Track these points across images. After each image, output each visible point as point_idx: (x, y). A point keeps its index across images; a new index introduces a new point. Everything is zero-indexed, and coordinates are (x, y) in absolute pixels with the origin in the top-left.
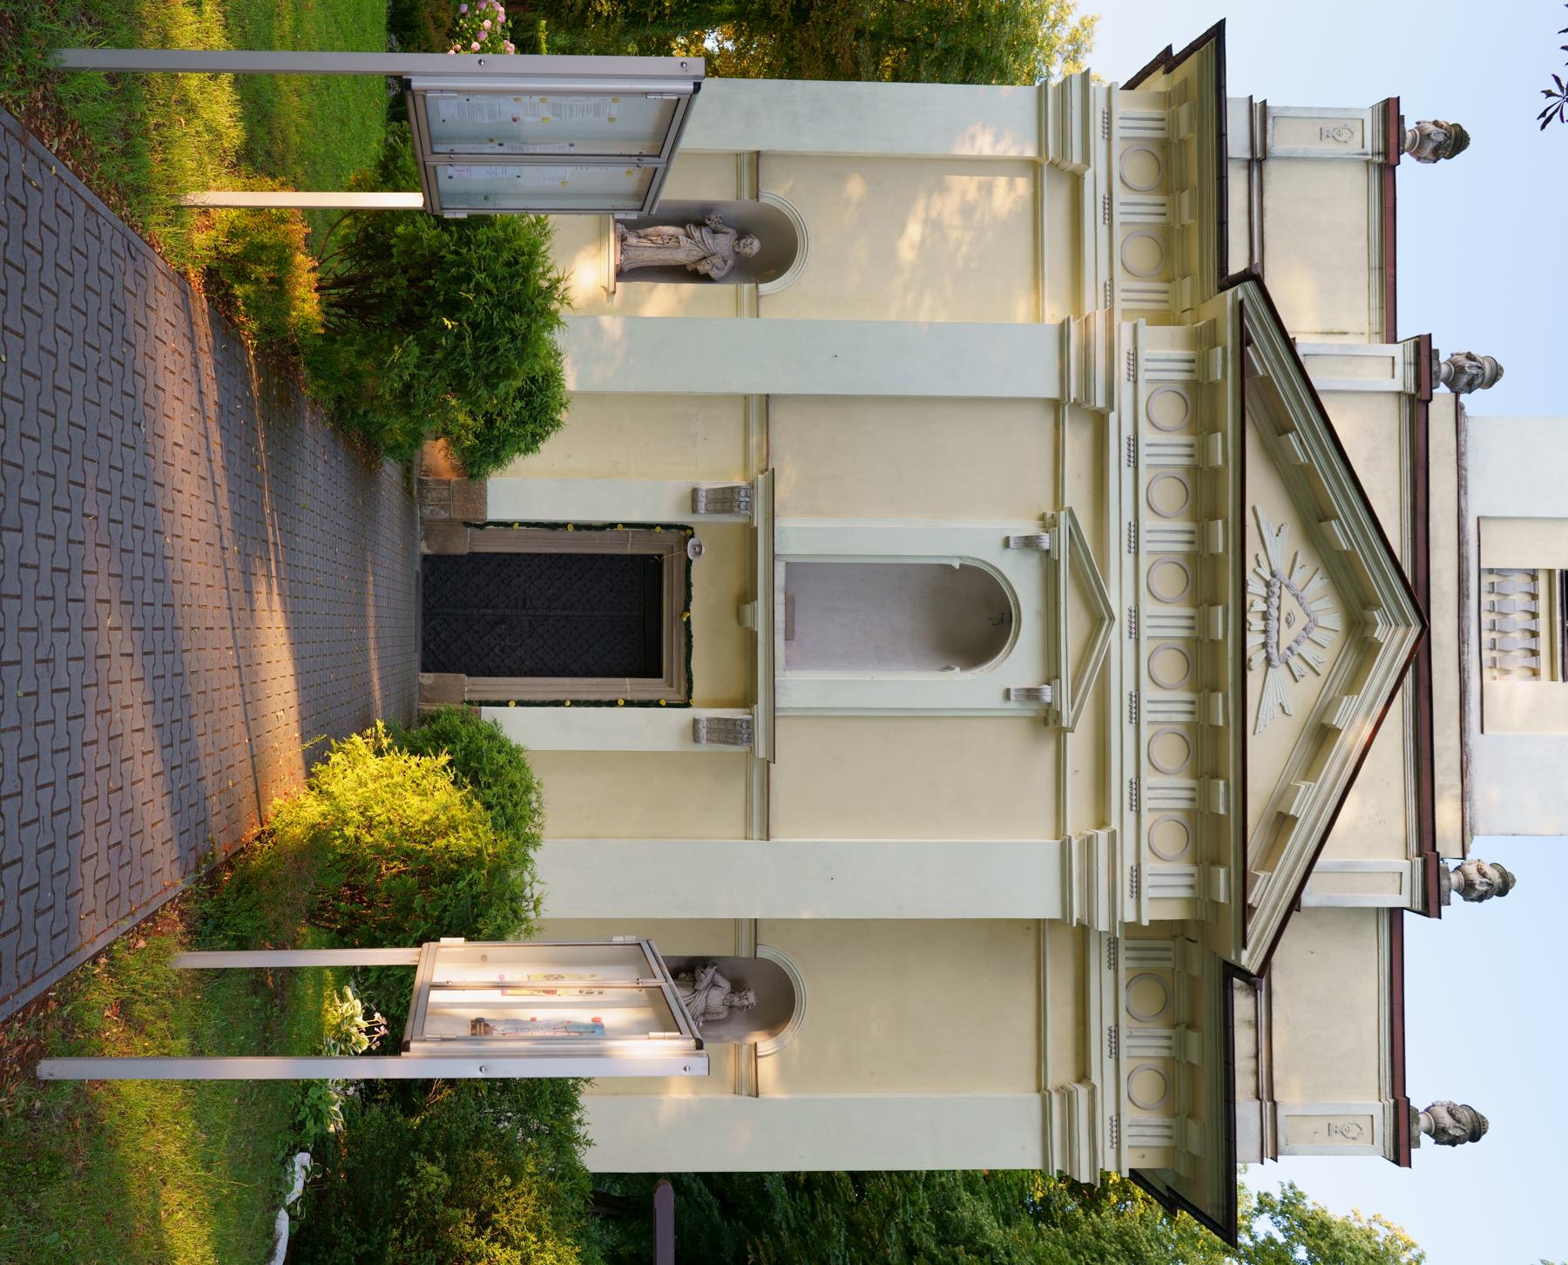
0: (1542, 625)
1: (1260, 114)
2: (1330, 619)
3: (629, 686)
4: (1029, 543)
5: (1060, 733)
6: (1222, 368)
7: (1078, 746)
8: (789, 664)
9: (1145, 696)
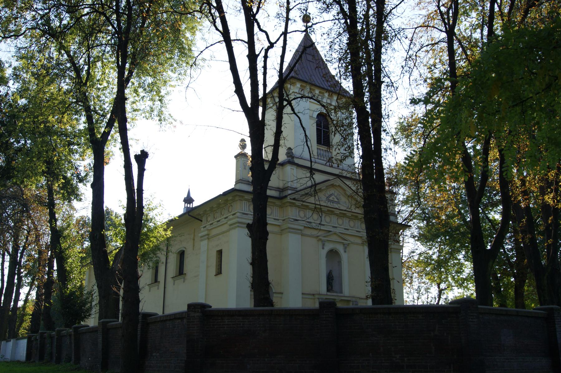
0: (321, 148)
1: (237, 182)
2: (332, 191)
4: (323, 245)
5: (352, 243)
6: (298, 203)
7: (352, 239)
8: (341, 292)
9: (275, 218)
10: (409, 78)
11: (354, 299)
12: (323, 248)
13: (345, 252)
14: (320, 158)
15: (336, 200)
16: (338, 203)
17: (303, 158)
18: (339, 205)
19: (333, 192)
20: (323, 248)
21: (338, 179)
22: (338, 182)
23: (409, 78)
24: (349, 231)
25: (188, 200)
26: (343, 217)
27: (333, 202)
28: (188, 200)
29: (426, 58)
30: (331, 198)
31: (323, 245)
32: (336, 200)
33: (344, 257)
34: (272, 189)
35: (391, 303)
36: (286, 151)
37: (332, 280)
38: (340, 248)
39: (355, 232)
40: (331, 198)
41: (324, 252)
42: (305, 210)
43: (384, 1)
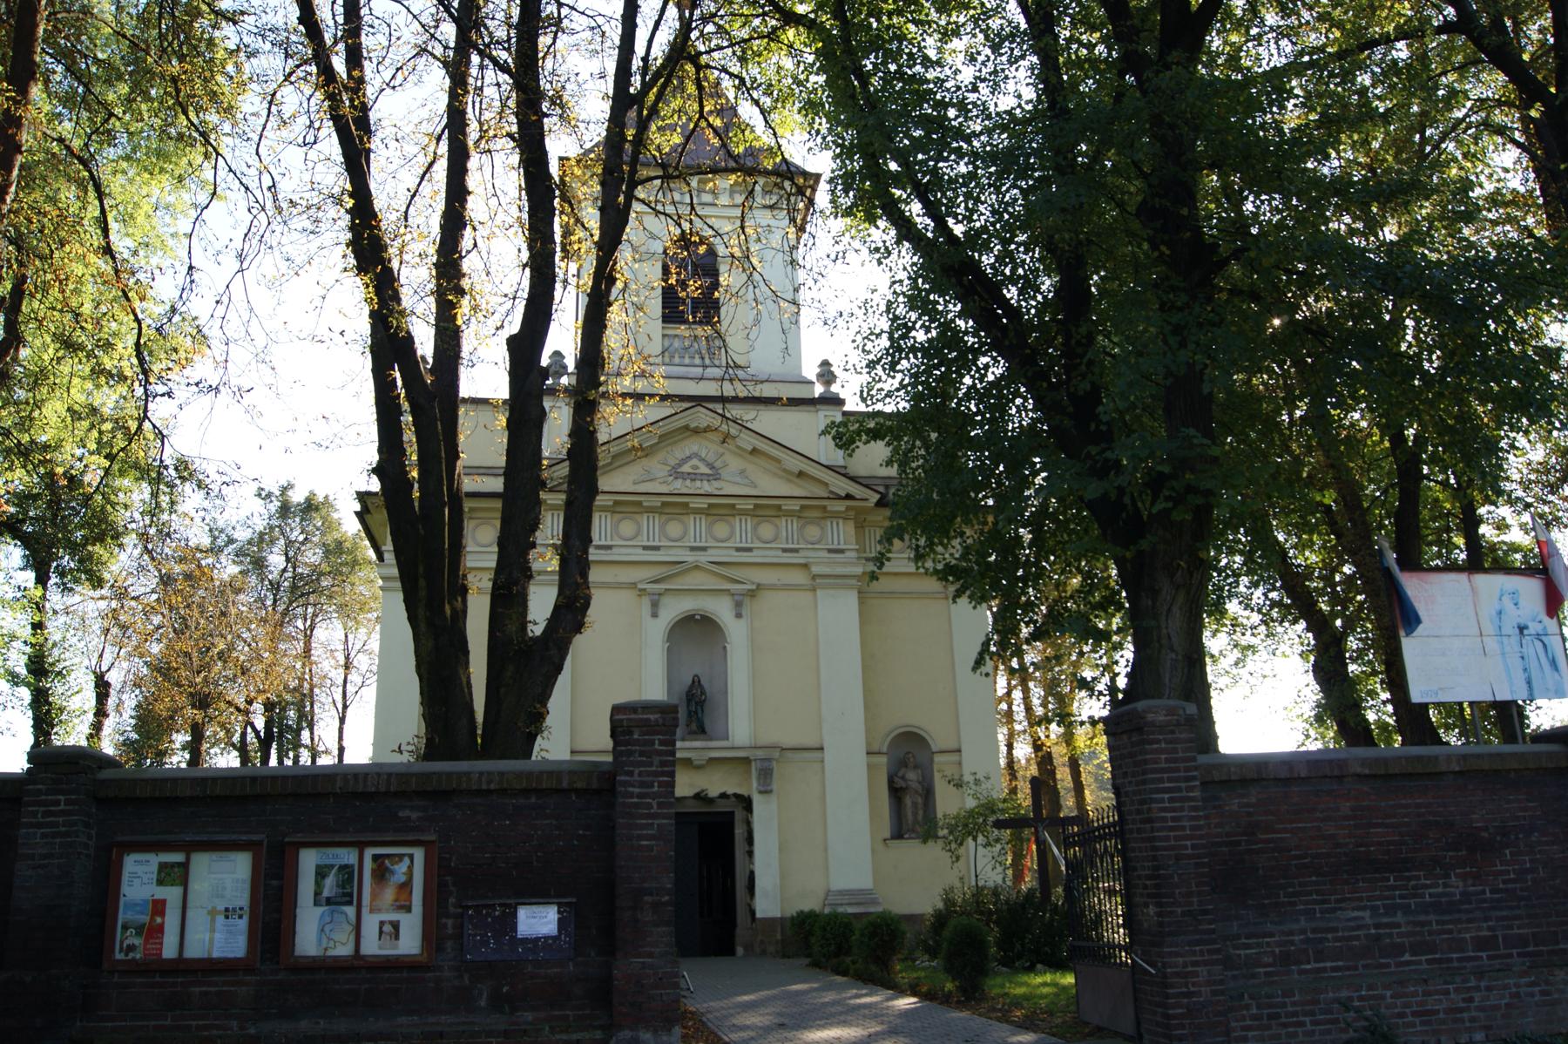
2: (692, 446)
3: (739, 831)
4: (655, 606)
10: (257, 154)
11: (760, 754)
12: (655, 615)
13: (739, 615)
14: (677, 360)
15: (704, 470)
16: (715, 476)
17: (772, 378)
18: (716, 484)
19: (695, 448)
20: (655, 615)
21: (700, 409)
22: (702, 417)
23: (257, 154)
24: (755, 553)
25: (975, 608)
26: (734, 515)
27: (693, 477)
28: (975, 608)
29: (291, 99)
30: (686, 468)
31: (655, 606)
32: (704, 470)
33: (736, 631)
34: (474, 470)
35: (727, 738)
36: (818, 370)
37: (701, 703)
38: (721, 610)
39: (780, 553)
40: (686, 468)
41: (656, 630)
42: (637, 516)
43: (358, 3)
